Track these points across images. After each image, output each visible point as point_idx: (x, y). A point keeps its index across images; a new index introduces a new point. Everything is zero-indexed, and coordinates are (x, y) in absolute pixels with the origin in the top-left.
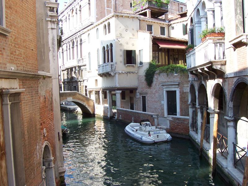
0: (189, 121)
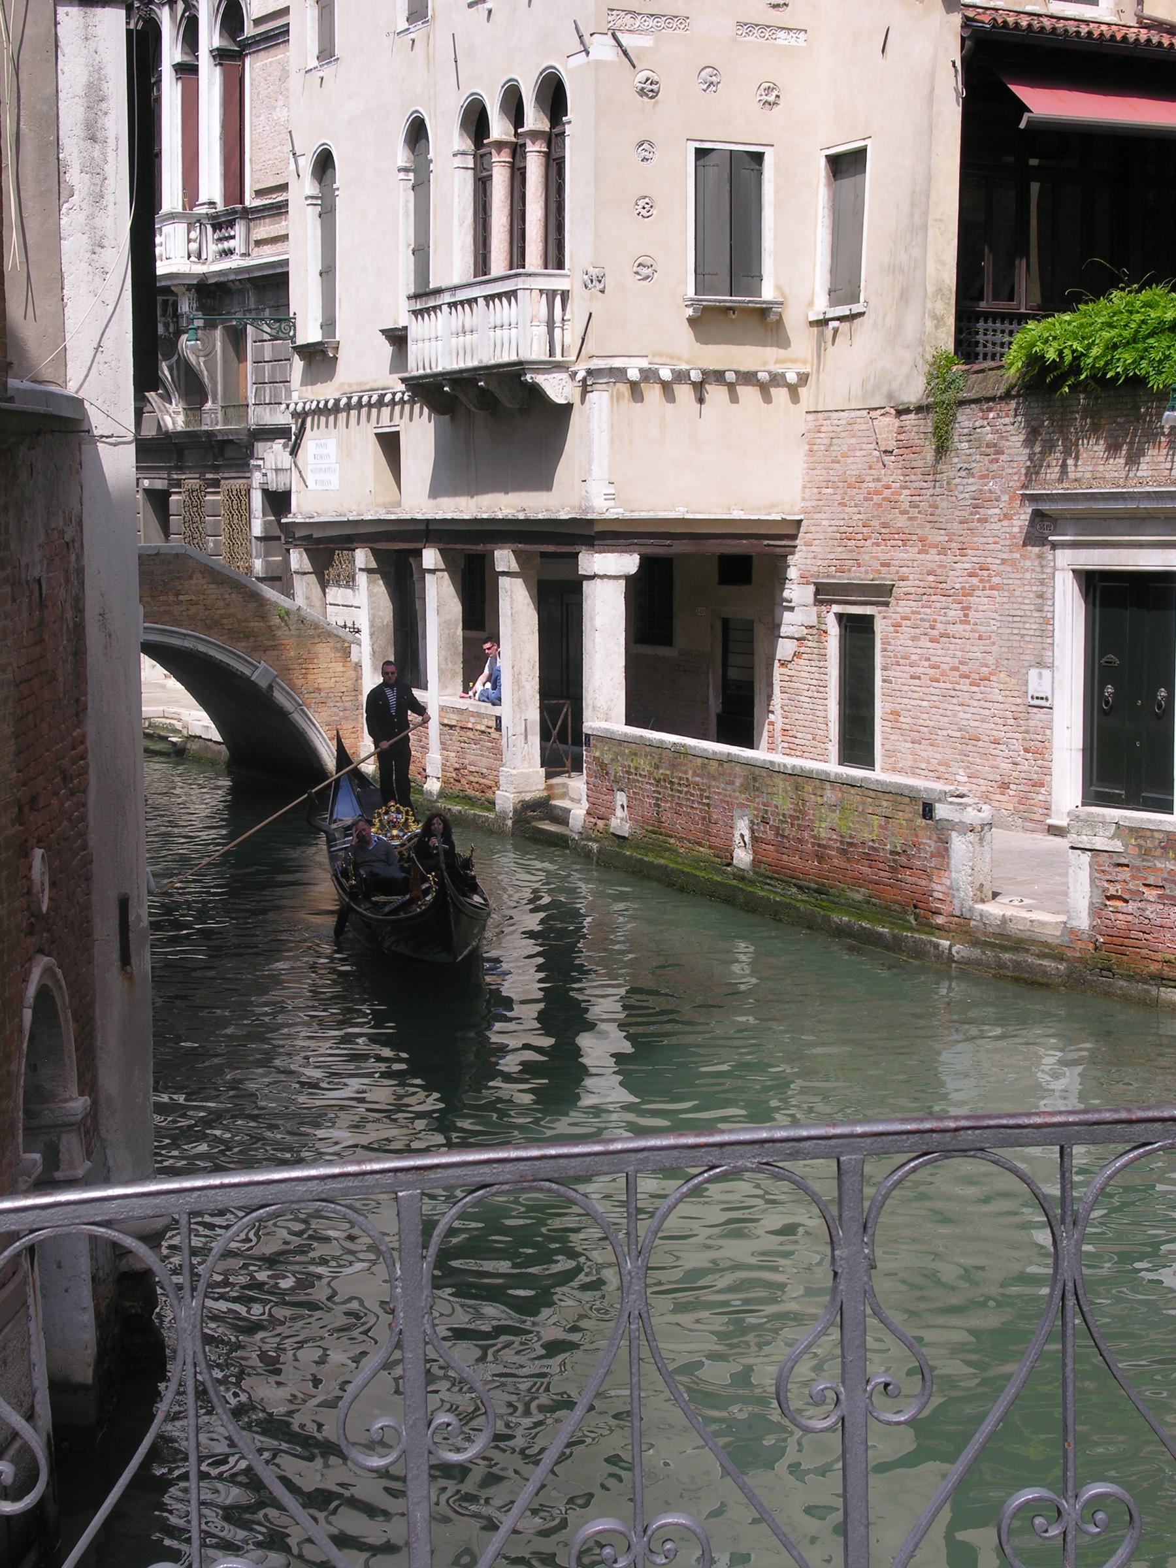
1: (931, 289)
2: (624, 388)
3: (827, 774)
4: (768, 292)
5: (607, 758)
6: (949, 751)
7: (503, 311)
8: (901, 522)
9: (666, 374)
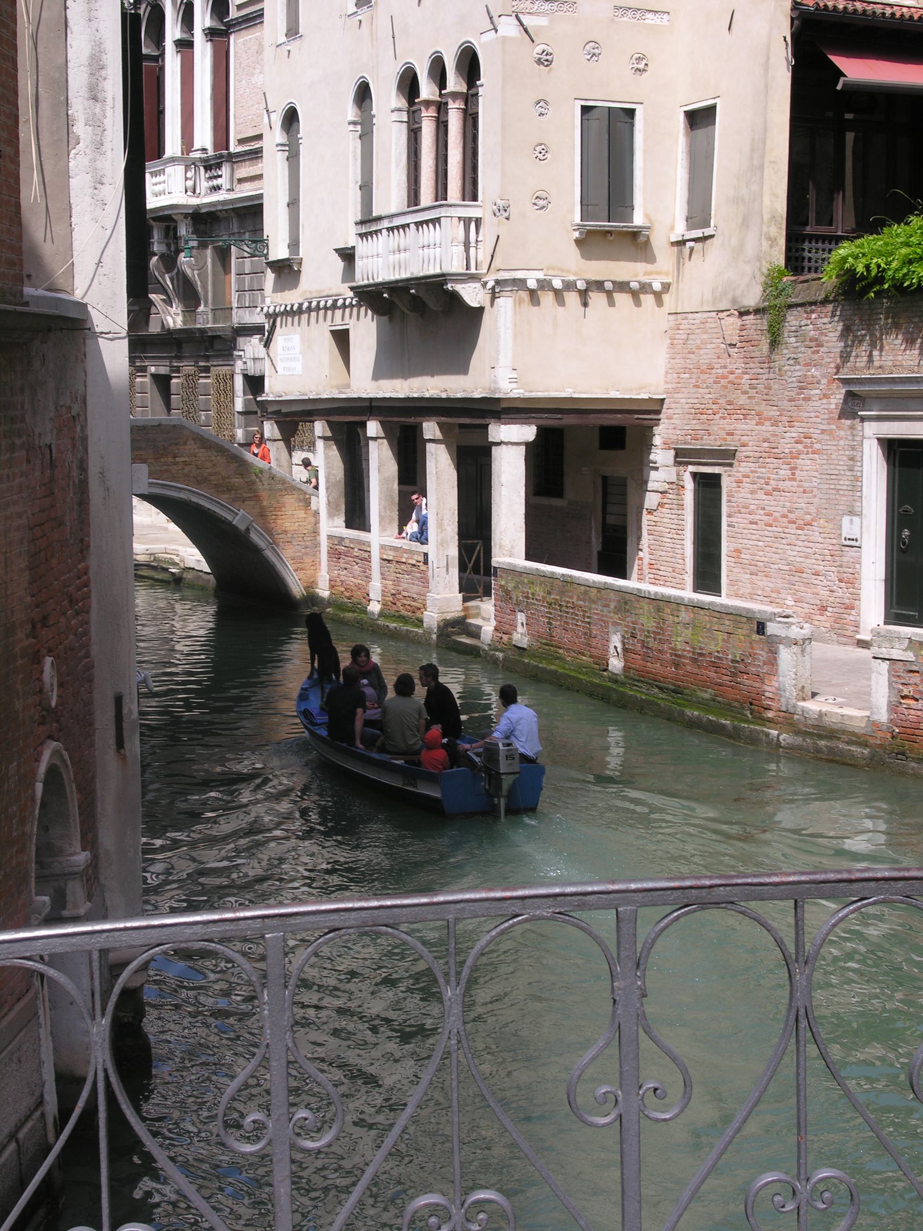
1: (766, 217)
2: (524, 295)
3: (682, 599)
4: (638, 219)
5: (510, 586)
6: (780, 581)
7: (430, 234)
8: (743, 400)
9: (557, 284)
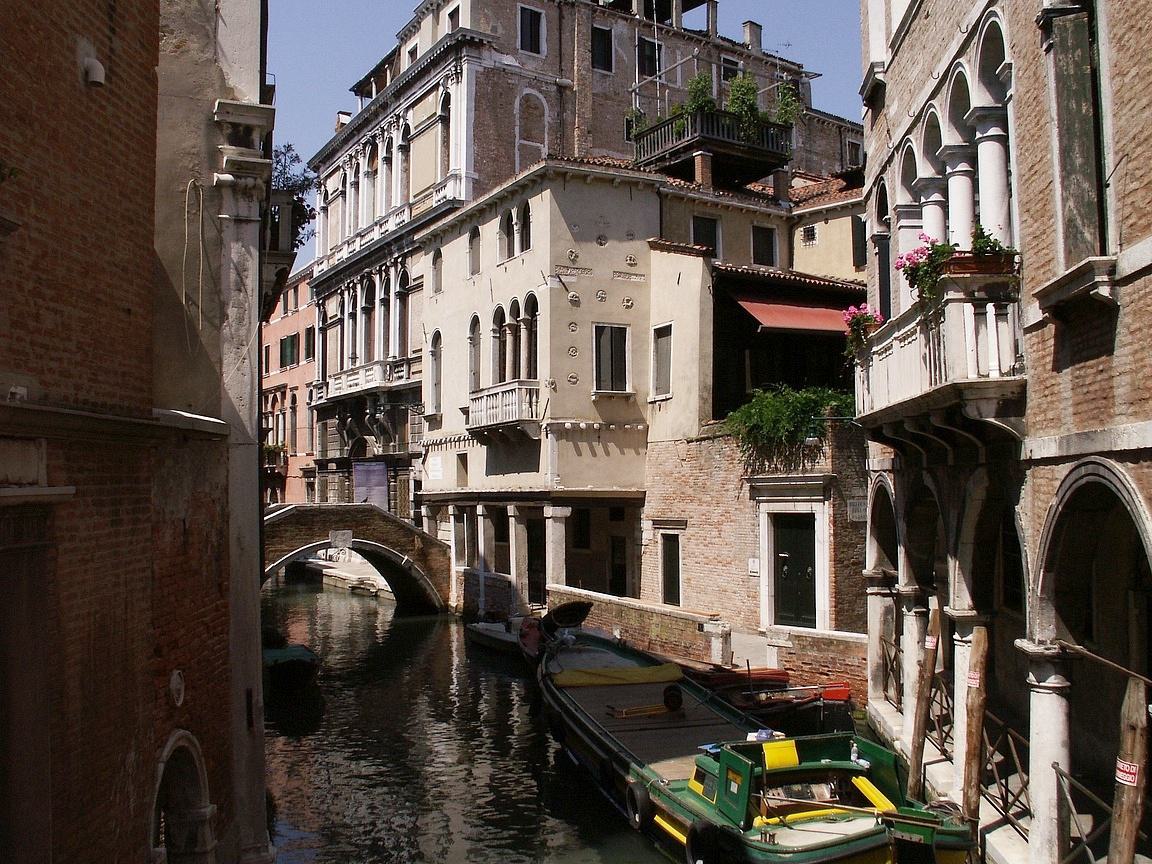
0: (866, 652)
4: (629, 389)
8: (690, 491)
